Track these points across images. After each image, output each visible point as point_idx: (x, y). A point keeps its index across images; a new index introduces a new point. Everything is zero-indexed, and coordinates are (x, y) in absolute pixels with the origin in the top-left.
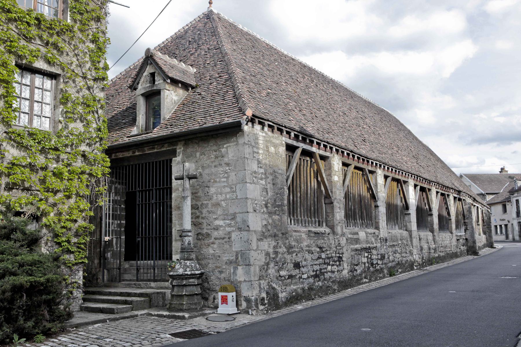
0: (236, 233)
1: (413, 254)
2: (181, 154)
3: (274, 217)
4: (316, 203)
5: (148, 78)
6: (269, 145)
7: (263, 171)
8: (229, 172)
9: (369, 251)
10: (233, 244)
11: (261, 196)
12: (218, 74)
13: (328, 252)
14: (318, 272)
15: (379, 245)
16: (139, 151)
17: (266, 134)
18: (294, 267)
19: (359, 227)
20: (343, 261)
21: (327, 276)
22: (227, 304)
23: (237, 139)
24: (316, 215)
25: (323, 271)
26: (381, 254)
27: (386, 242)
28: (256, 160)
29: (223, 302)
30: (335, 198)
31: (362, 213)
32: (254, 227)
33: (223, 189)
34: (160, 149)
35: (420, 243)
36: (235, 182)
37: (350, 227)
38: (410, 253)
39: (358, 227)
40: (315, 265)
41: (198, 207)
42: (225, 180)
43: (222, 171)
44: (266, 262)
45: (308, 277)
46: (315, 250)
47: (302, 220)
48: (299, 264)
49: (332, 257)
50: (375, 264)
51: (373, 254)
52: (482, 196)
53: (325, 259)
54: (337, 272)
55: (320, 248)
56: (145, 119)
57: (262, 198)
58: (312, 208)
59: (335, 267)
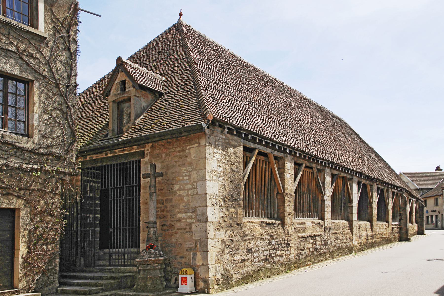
0: (195, 224)
2: (149, 156)
14: (268, 257)
17: (226, 136)
20: (290, 247)
22: (186, 285)
23: (199, 140)
29: (183, 283)
36: (196, 180)
41: (163, 202)
42: (187, 178)
43: (185, 170)
44: (222, 248)
48: (251, 250)
52: (417, 191)
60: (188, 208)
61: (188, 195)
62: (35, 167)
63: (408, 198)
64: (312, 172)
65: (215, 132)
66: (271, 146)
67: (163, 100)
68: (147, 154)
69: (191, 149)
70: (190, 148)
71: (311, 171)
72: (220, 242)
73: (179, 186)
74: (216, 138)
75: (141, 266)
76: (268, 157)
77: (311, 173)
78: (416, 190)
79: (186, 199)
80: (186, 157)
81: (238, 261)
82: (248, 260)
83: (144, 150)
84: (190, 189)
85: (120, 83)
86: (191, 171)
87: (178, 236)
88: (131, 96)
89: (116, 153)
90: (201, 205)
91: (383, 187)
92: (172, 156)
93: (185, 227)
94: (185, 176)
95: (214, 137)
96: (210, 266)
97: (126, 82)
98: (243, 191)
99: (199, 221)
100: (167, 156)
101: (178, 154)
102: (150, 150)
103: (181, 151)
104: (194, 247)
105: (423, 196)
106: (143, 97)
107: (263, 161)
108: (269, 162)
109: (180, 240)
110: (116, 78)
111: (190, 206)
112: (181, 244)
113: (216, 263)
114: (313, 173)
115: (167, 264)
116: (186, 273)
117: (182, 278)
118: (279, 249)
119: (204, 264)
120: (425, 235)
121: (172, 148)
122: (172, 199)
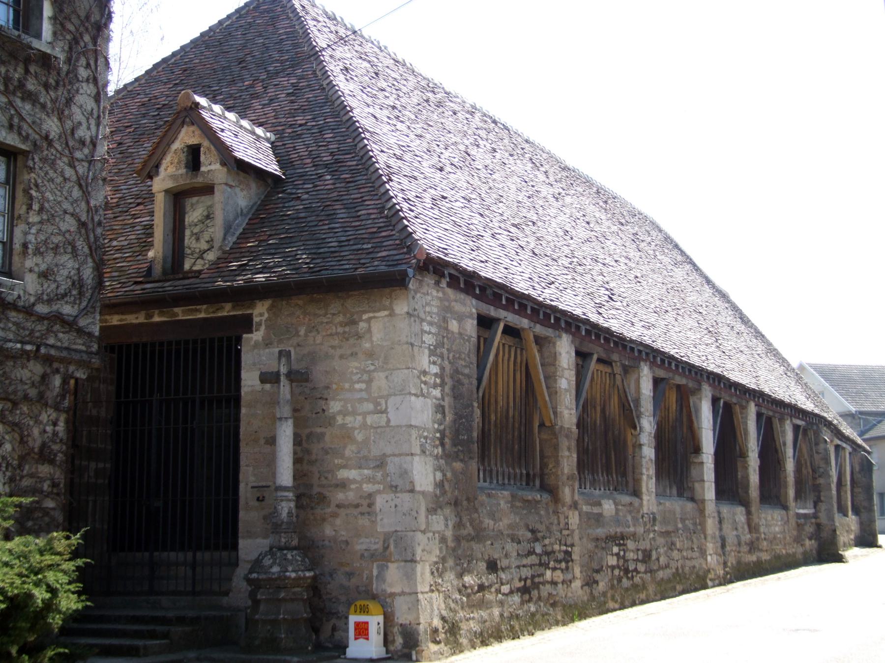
0: (384, 496)
1: (705, 551)
2: (263, 328)
3: (454, 464)
4: (523, 436)
5: (183, 157)
6: (449, 315)
7: (438, 371)
8: (374, 371)
9: (622, 542)
10: (379, 518)
11: (434, 422)
12: (332, 154)
13: (547, 541)
14: (529, 582)
15: (640, 530)
16: (161, 314)
17: (444, 293)
18: (488, 568)
19: (602, 489)
20: (572, 561)
21: (546, 590)
22: (367, 639)
23: (391, 303)
24: (523, 462)
25: (537, 580)
26: (644, 551)
27: (654, 525)
28: (426, 348)
29: (360, 634)
30: (562, 427)
31: (608, 458)
32: (421, 485)
33: (357, 404)
34: (214, 312)
35: (721, 529)
36: (385, 393)
37: (585, 488)
38: (701, 549)
39: (600, 489)
40: (524, 566)
41: (301, 440)
42: (363, 386)
43: (356, 368)
44: (442, 555)
45: (511, 592)
46: (523, 535)
47: (509, 473)
48: (496, 564)
49: (553, 552)
50: (633, 571)
51: (628, 549)
52: (850, 419)
53: (540, 555)
54: (563, 584)
55: (533, 531)
56: (171, 243)
57: (436, 426)
58: (516, 447)
59: (558, 573)
60: (366, 458)
61: (364, 426)
62: (28, 347)
63: (832, 441)
64: (610, 374)
65: (424, 284)
66: (504, 302)
67: (286, 196)
68: (259, 324)
69: (373, 321)
70: (370, 318)
71: (609, 370)
72: (437, 541)
73: (342, 403)
74: (427, 297)
75: (261, 590)
76: (521, 339)
77: (608, 375)
78: (847, 416)
79: (359, 437)
80: (359, 337)
81: (472, 587)
82: (490, 586)
83: (252, 314)
84: (369, 413)
85: (185, 150)
86: (374, 371)
87: (338, 522)
88: (214, 184)
89: (176, 315)
90: (397, 452)
91: (771, 413)
92: (324, 334)
93: (355, 503)
94: (358, 382)
95: (422, 295)
96: (420, 596)
97: (202, 149)
98: (477, 420)
99: (394, 488)
100: (310, 332)
101: (340, 330)
102: (266, 315)
103: (346, 324)
104: (381, 550)
105: (867, 436)
106: (241, 186)
107: (510, 346)
108: (522, 349)
109: (343, 533)
110: (176, 138)
111: (369, 452)
112: (347, 543)
113: (432, 591)
114: (613, 375)
115: (315, 588)
116: (364, 610)
117: (357, 624)
118: (550, 566)
119: (407, 590)
120: (880, 547)
121: (325, 315)
122: (323, 435)
